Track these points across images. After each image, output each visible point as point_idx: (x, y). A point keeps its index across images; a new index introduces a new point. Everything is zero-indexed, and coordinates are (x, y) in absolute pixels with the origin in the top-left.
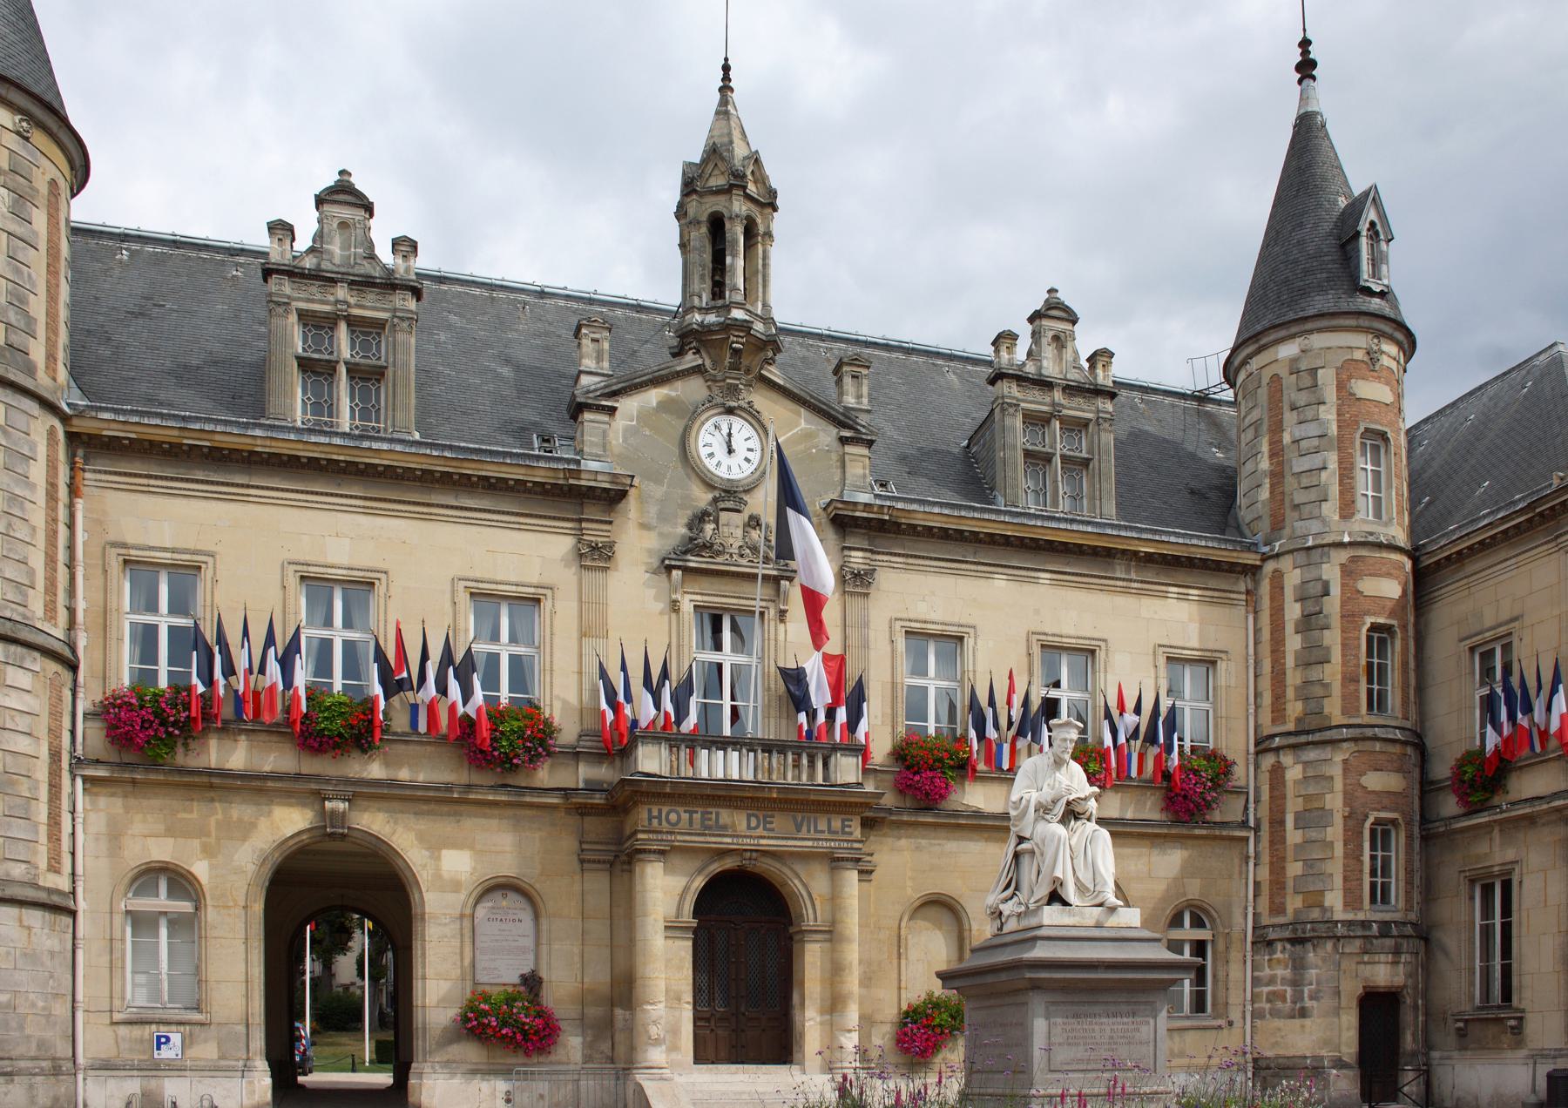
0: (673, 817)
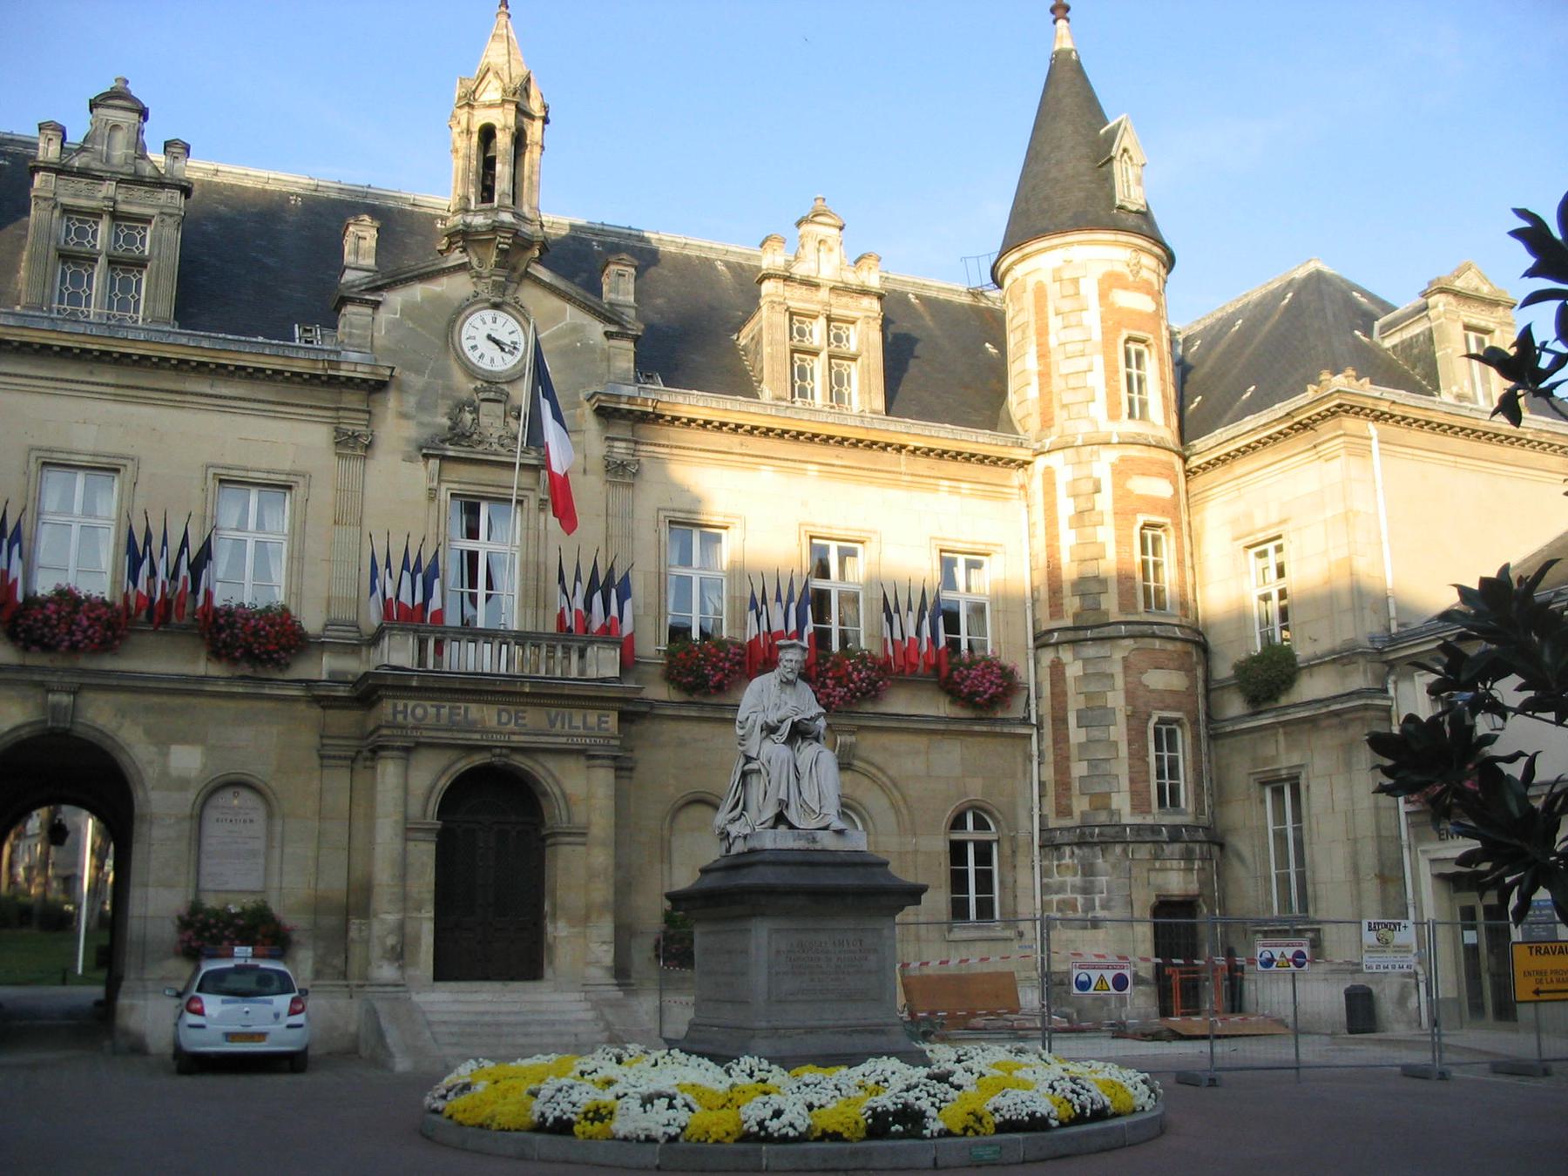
0: (419, 712)
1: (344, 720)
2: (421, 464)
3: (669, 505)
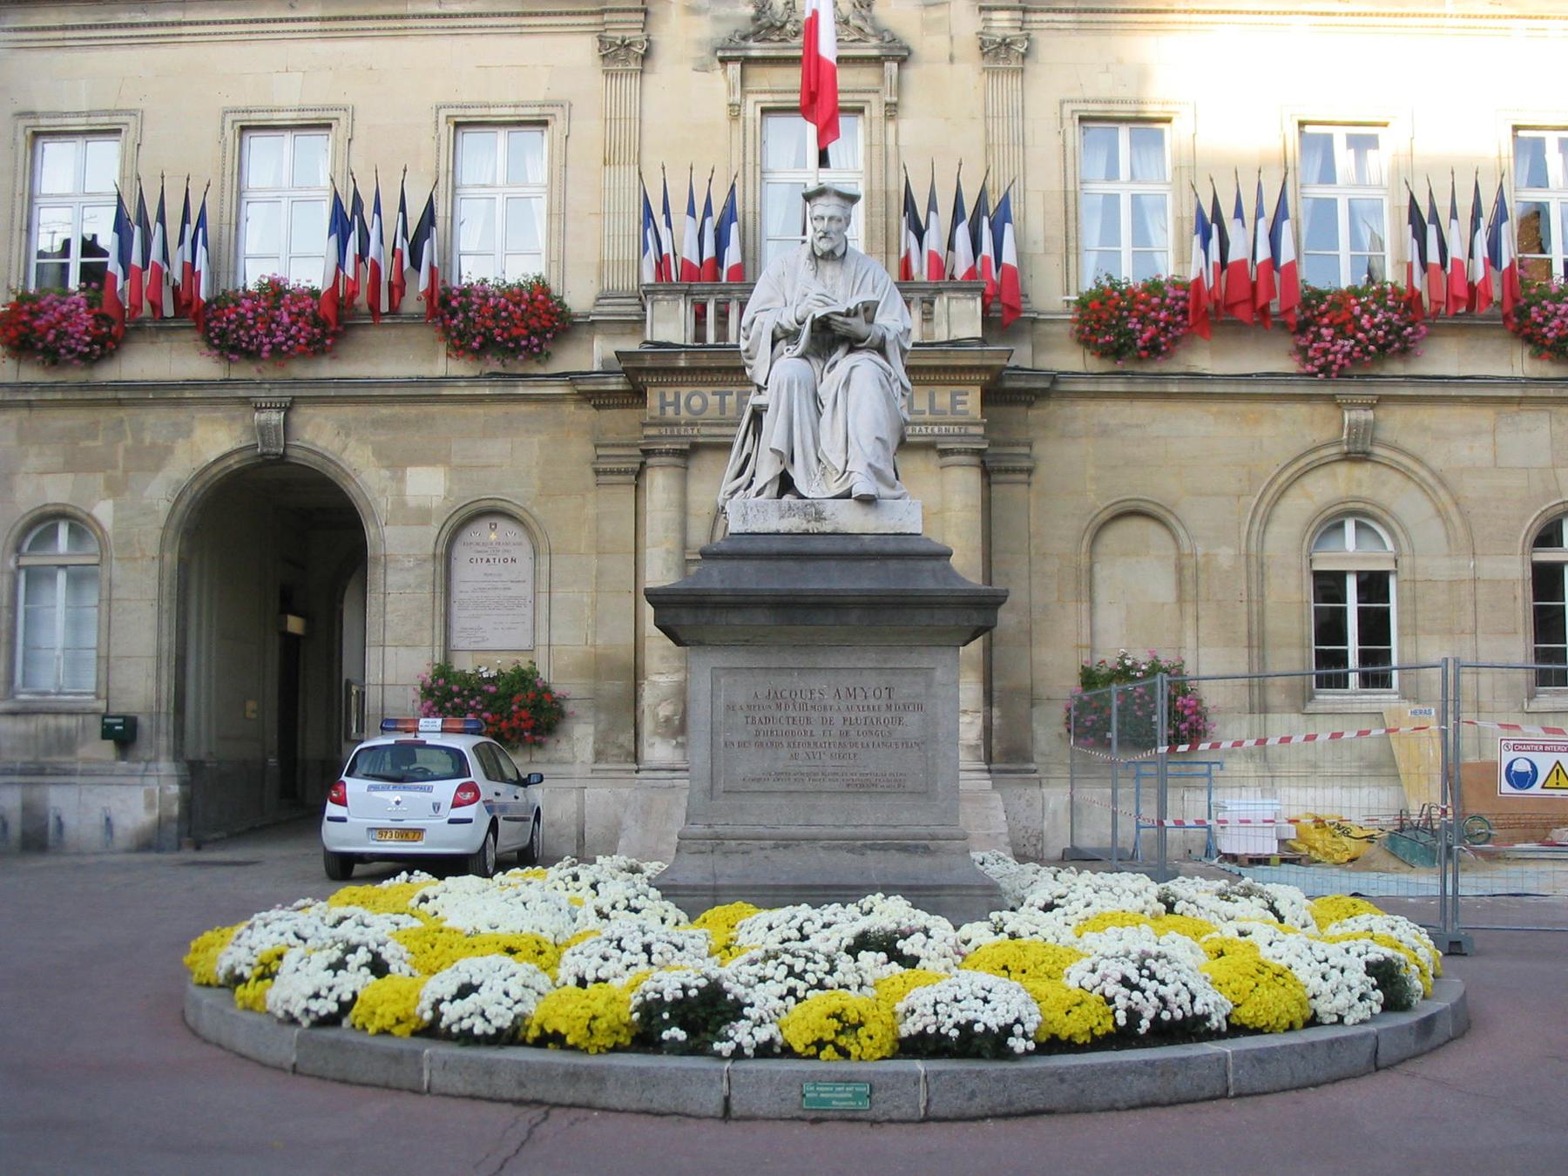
0: (696, 402)
1: (619, 421)
2: (719, 72)
3: (1077, 95)
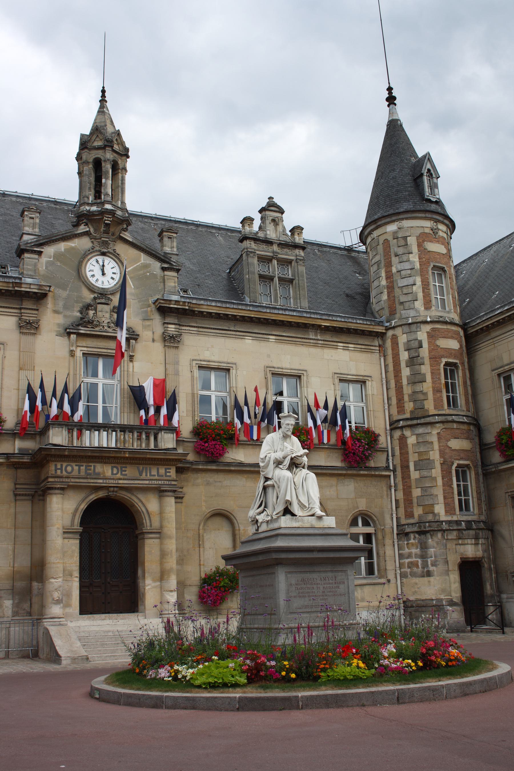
0: (69, 469)
3: (198, 358)
